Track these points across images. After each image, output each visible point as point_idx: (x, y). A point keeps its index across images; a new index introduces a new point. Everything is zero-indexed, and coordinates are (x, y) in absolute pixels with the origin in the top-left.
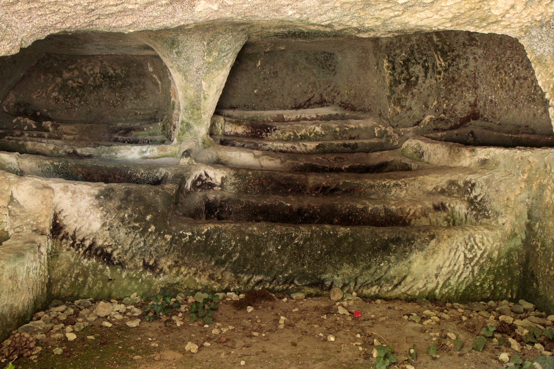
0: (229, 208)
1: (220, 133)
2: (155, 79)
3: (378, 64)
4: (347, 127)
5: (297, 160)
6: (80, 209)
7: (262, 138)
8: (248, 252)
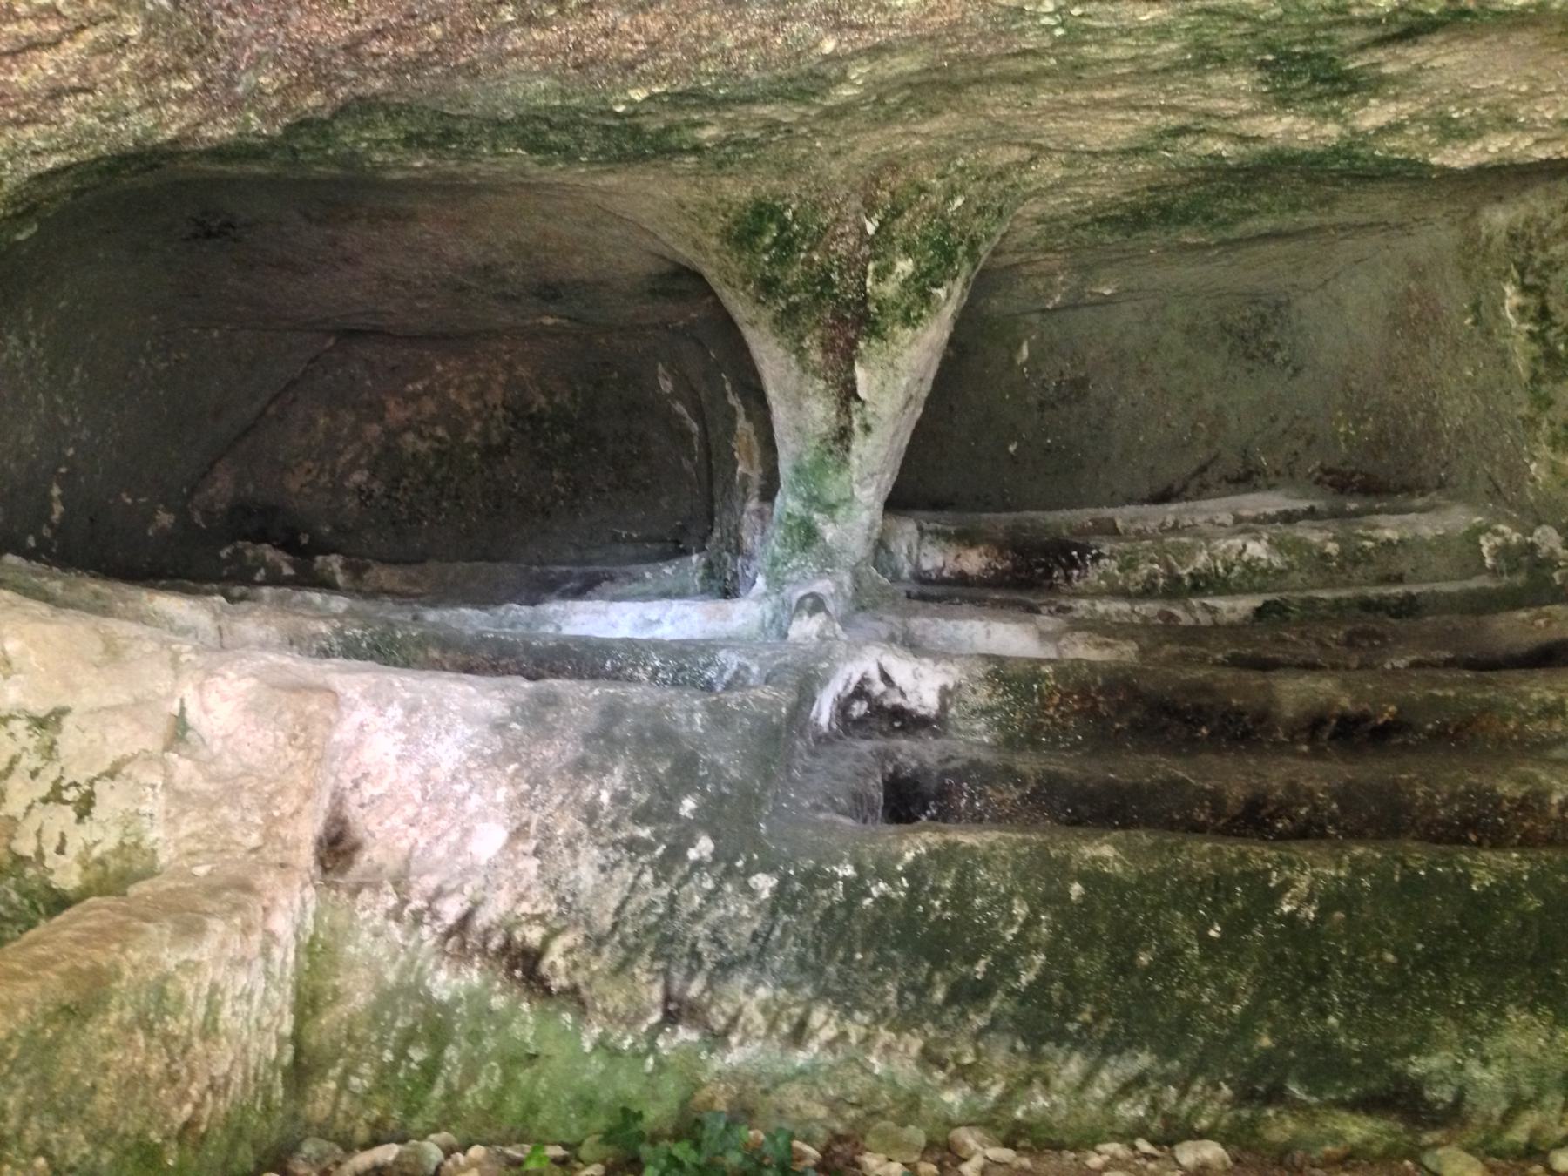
0: (971, 801)
1: (906, 574)
2: (679, 417)
3: (1476, 308)
4: (1369, 538)
5: (1201, 644)
6: (434, 773)
7: (1053, 588)
8: (1083, 948)
